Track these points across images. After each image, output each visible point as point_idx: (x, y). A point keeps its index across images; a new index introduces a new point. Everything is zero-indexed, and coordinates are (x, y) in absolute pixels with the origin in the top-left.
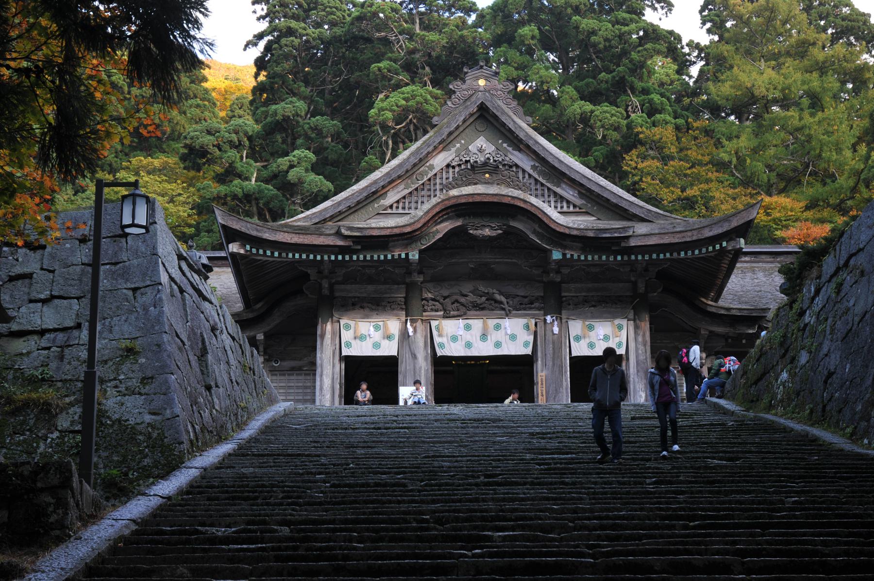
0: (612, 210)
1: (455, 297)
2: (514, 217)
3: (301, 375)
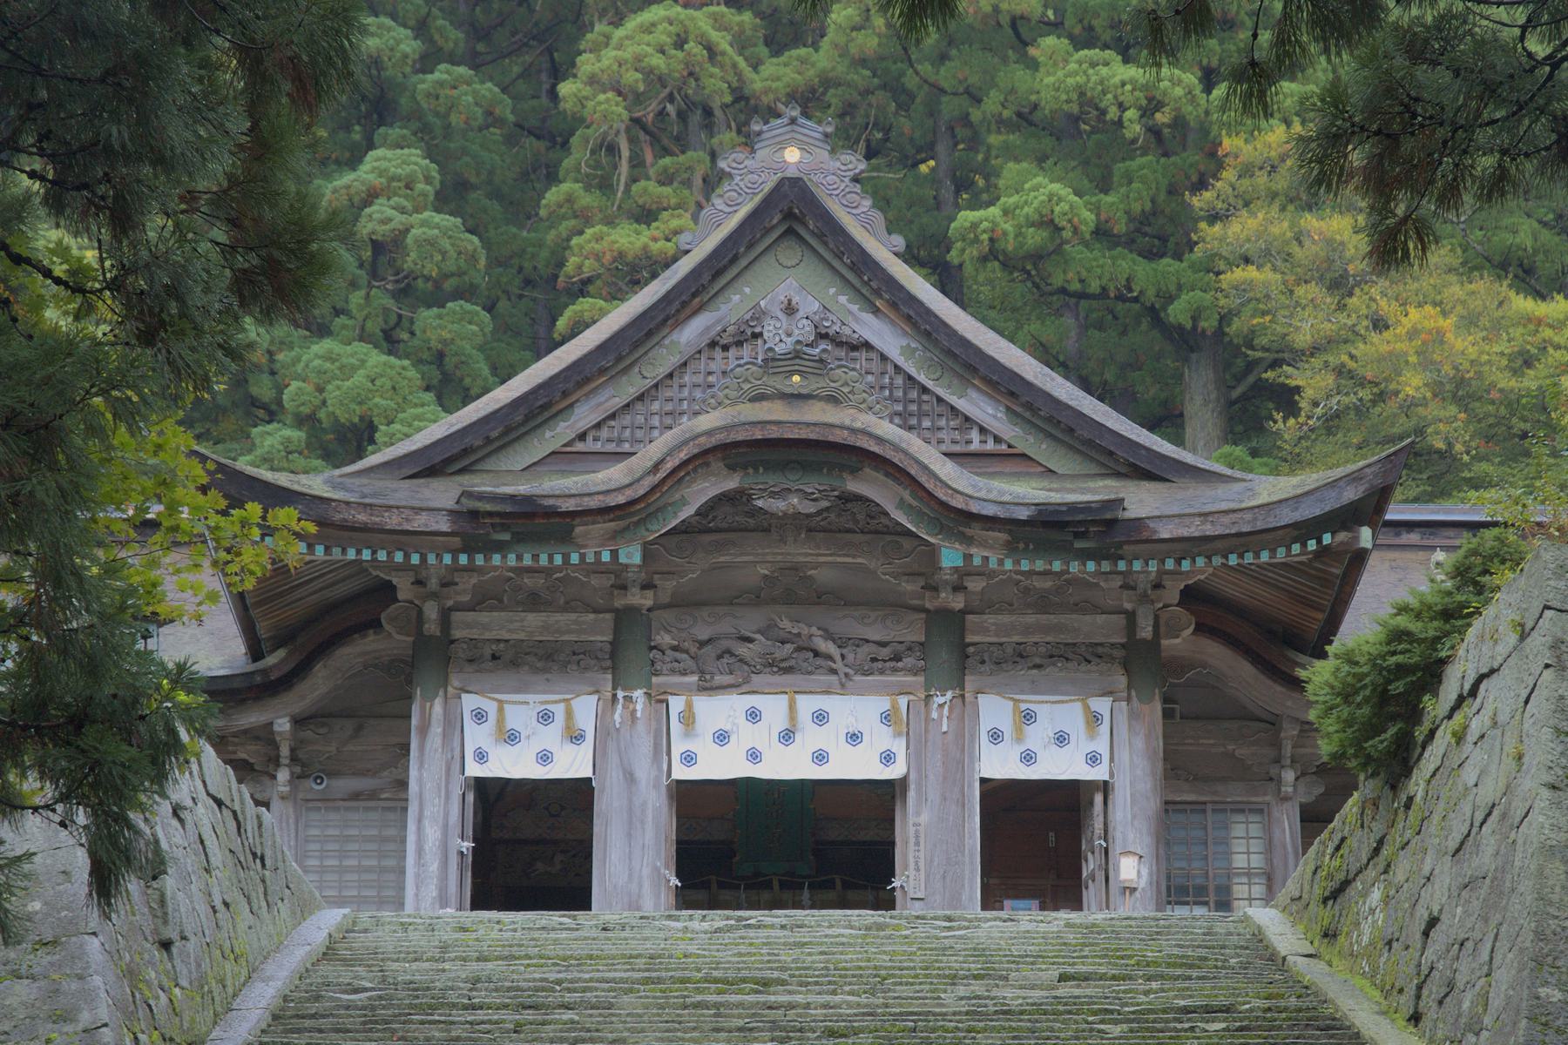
0: (1079, 452)
1: (725, 644)
2: (854, 471)
3: (375, 809)
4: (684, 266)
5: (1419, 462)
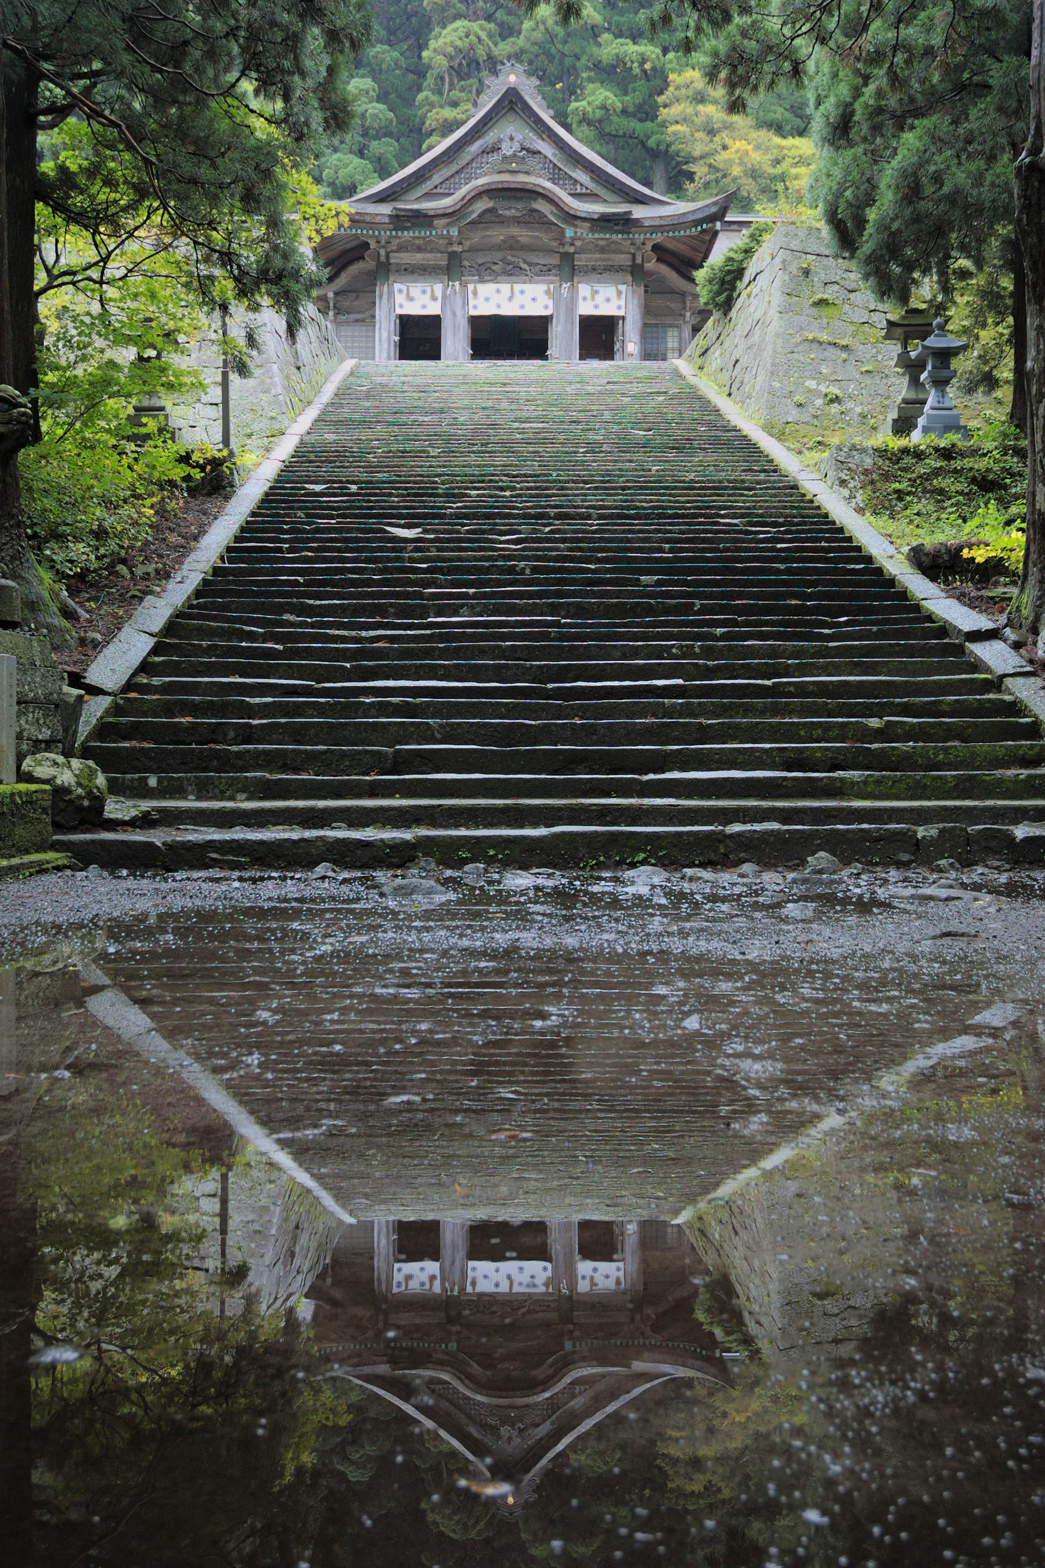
5: (732, 200)
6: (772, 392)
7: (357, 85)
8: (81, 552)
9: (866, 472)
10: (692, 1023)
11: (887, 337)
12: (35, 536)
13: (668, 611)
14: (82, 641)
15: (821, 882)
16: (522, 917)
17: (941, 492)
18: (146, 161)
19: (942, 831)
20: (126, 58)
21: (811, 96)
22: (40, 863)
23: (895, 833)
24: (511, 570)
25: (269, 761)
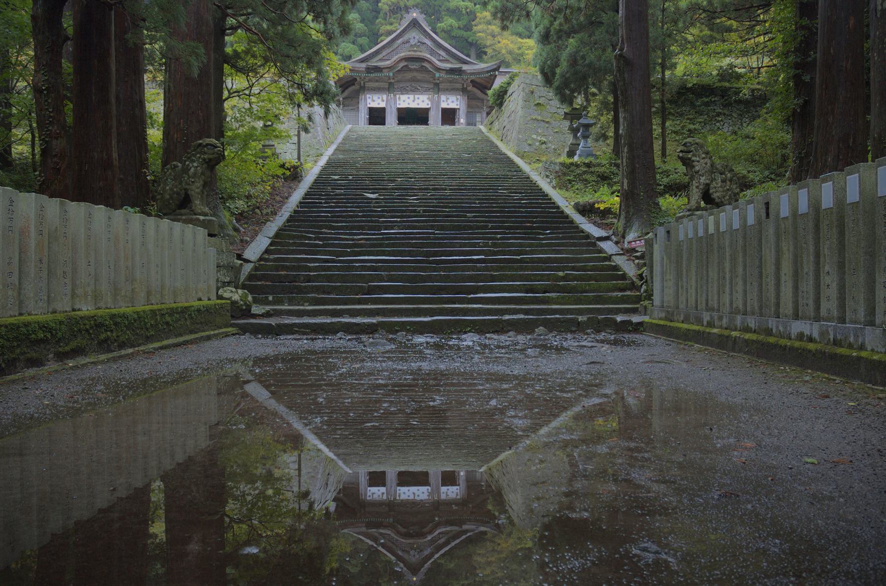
4: (398, 31)
5: (503, 63)
6: (519, 140)
7: (353, 17)
8: (241, 204)
9: (556, 172)
10: (493, 402)
11: (565, 118)
12: (223, 198)
13: (478, 228)
14: (242, 241)
15: (541, 340)
16: (423, 358)
17: (586, 180)
18: (269, 48)
19: (589, 318)
20: (262, 9)
21: (533, 24)
22: (226, 332)
23: (570, 319)
24: (415, 211)
25: (317, 290)
